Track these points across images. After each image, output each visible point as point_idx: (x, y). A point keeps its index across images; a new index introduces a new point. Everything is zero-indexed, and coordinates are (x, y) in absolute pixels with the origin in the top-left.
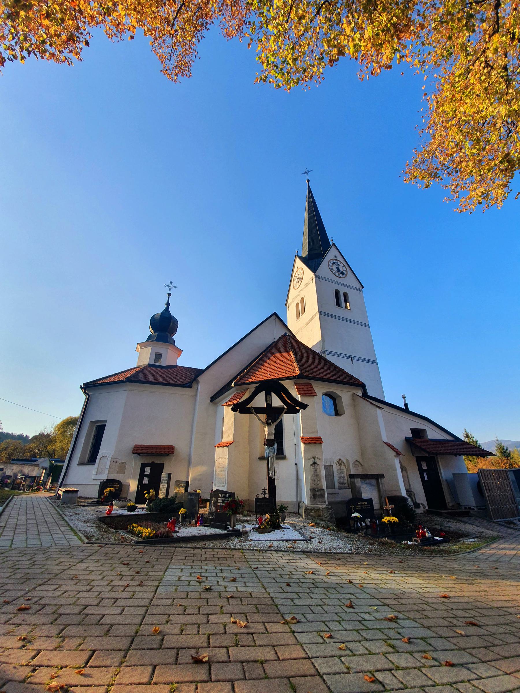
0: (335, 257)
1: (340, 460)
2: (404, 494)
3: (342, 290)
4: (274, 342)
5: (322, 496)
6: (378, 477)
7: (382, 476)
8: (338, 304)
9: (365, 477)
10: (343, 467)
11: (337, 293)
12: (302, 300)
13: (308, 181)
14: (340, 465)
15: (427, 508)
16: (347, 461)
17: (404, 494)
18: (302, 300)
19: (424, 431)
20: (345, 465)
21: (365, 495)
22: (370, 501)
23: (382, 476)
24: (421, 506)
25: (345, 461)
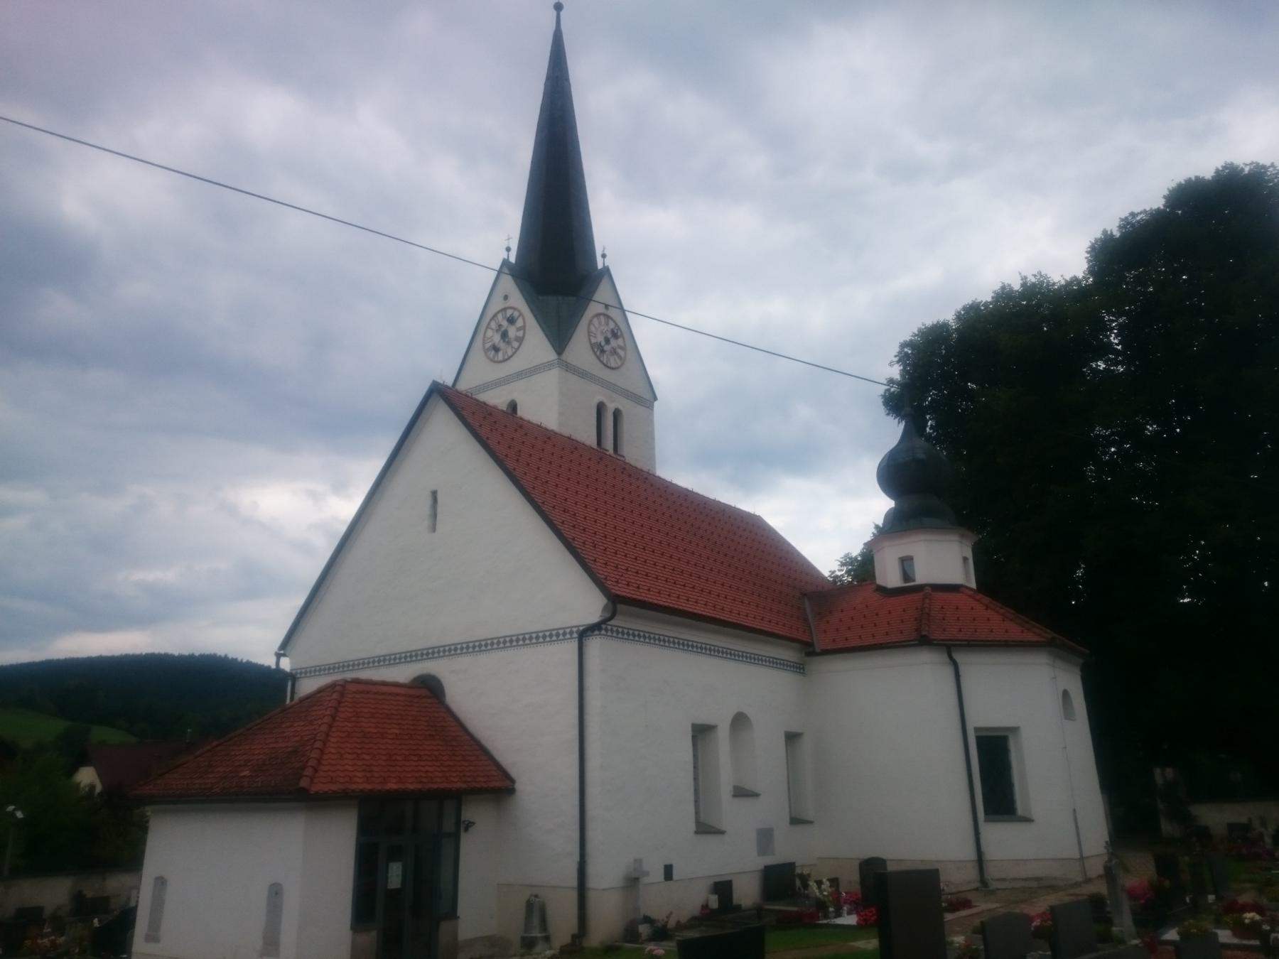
11: (600, 409)
13: (558, 7)
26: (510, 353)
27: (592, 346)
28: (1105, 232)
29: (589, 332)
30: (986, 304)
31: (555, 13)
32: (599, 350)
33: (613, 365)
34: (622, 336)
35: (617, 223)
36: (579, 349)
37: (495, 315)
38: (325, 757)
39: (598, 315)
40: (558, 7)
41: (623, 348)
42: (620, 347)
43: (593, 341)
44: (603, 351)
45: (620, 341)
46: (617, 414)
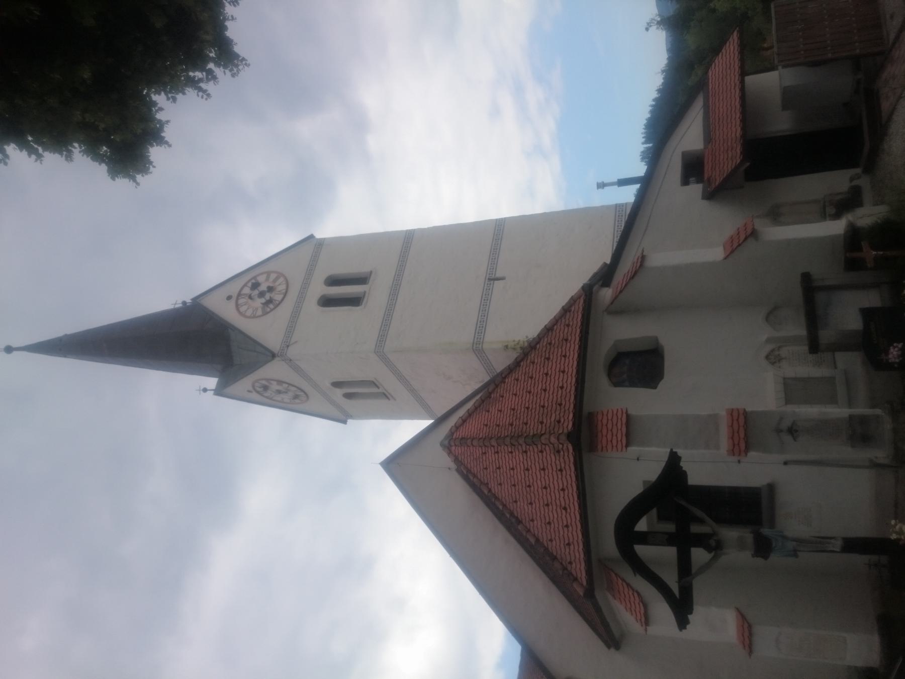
0: (229, 298)
1: (767, 357)
2: (836, 227)
3: (318, 289)
4: (458, 470)
5: (863, 420)
6: (809, 287)
7: (806, 278)
8: (354, 301)
9: (813, 319)
10: (784, 352)
11: (327, 302)
12: (337, 384)
13: (9, 350)
14: (780, 359)
15: (858, 171)
16: (769, 341)
17: (836, 227)
18: (337, 384)
19: (685, 155)
20: (780, 347)
21: (853, 322)
22: (867, 314)
23: (806, 278)
24: (855, 183)
25: (769, 347)
26: (293, 389)
27: (265, 313)
28: (113, 179)
29: (254, 317)
30: (152, 146)
31: (15, 353)
32: (270, 304)
33: (283, 287)
34: (255, 278)
35: (153, 296)
36: (265, 329)
37: (267, 397)
38: (574, 573)
39: (237, 306)
40: (9, 350)
41: (268, 274)
42: (267, 280)
43: (259, 312)
44: (270, 301)
45: (261, 279)
46: (333, 281)
